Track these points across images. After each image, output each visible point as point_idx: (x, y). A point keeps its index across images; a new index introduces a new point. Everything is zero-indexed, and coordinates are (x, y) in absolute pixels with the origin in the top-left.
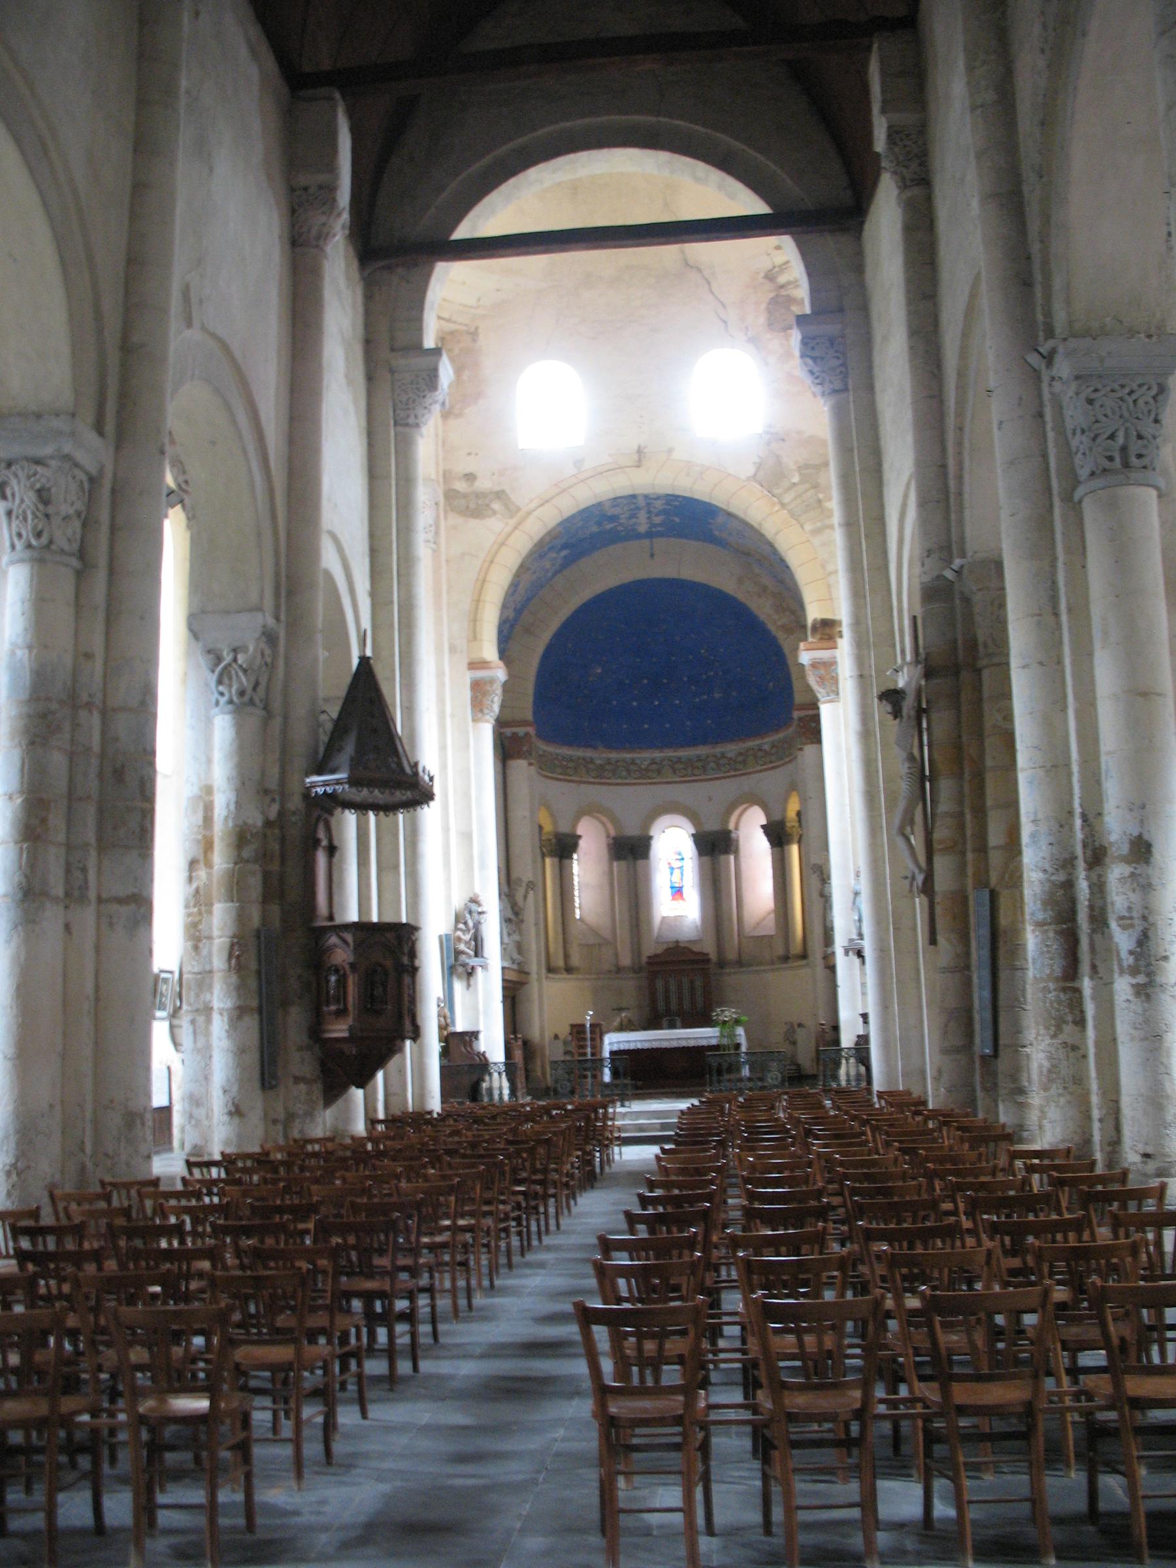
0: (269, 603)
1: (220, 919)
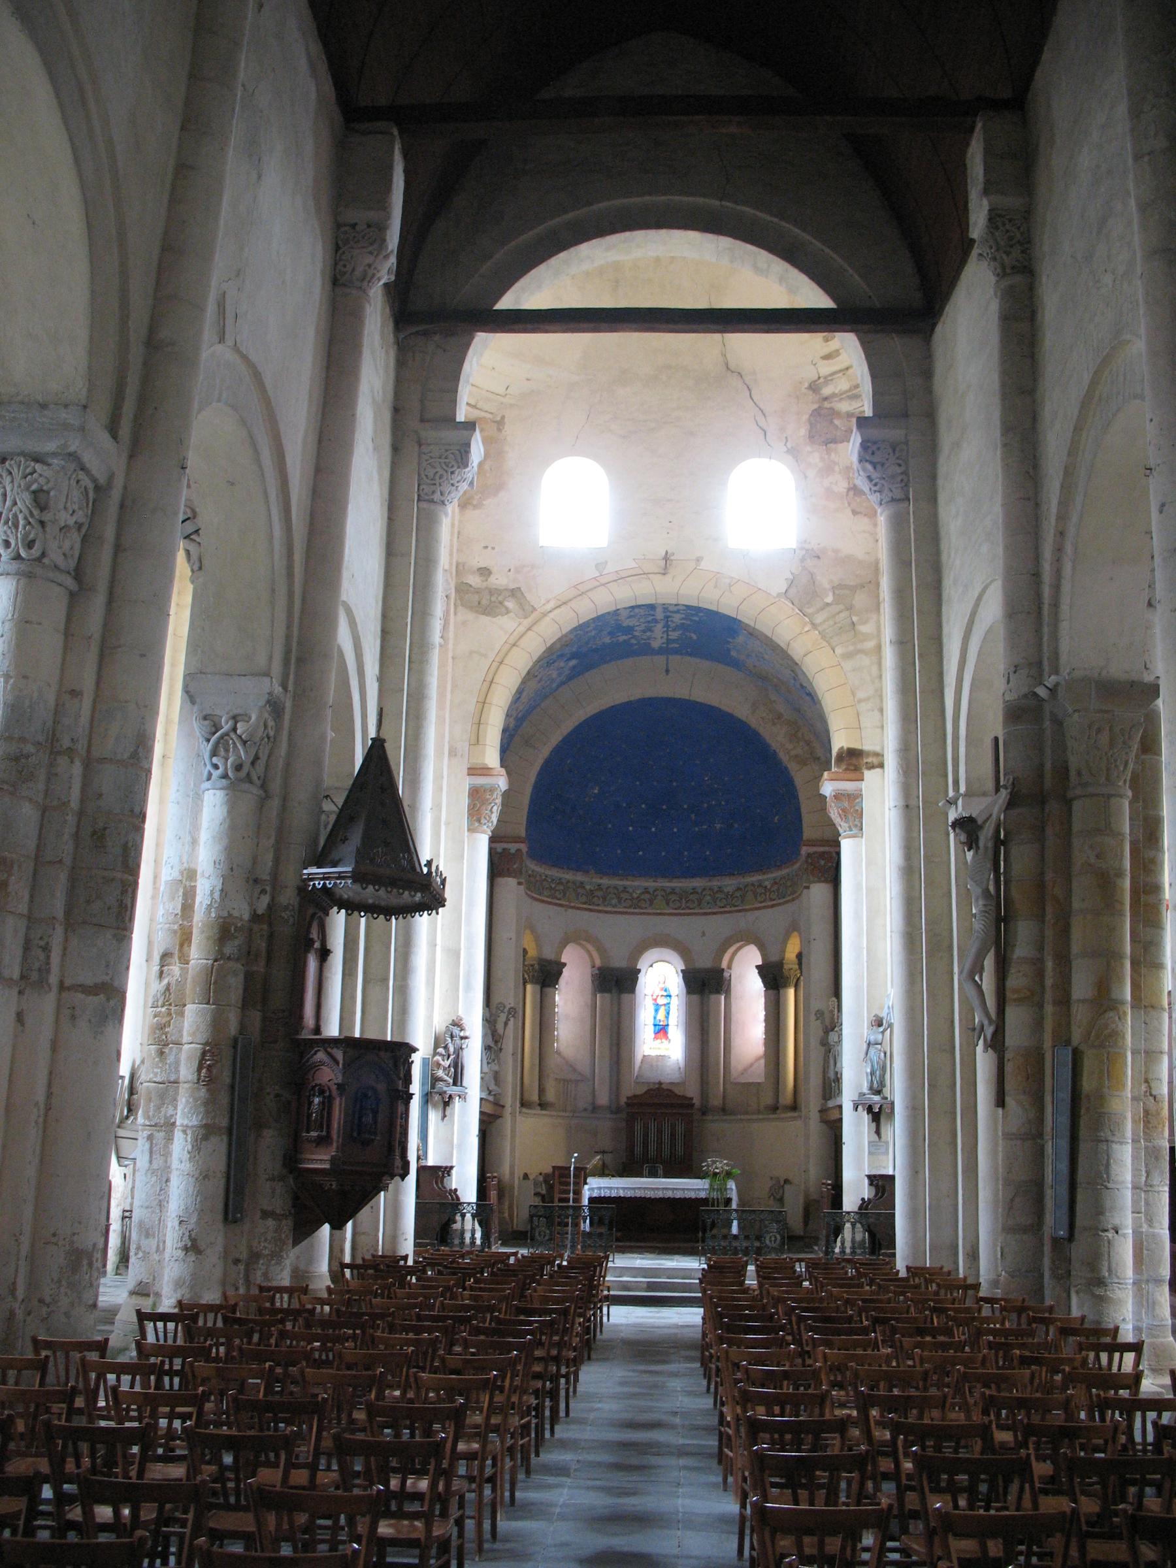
0: (277, 668)
1: (192, 1022)
